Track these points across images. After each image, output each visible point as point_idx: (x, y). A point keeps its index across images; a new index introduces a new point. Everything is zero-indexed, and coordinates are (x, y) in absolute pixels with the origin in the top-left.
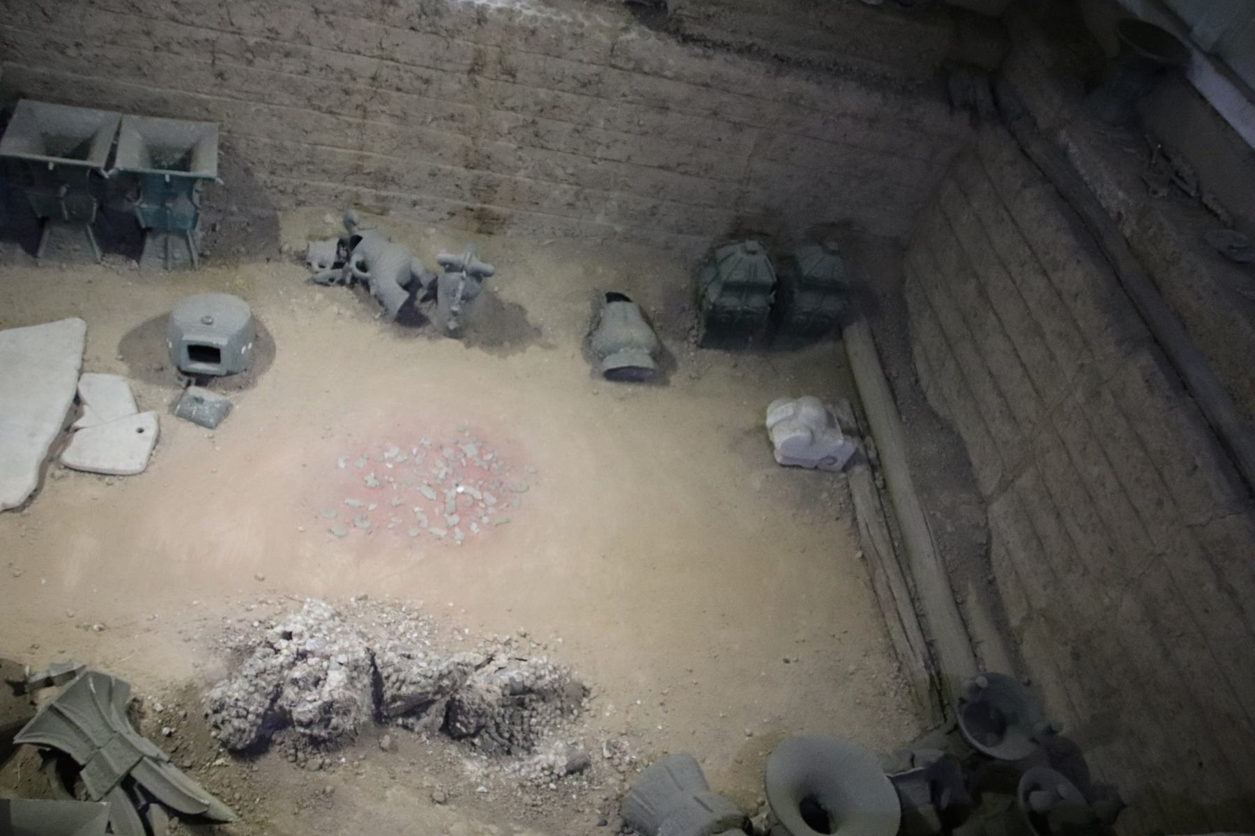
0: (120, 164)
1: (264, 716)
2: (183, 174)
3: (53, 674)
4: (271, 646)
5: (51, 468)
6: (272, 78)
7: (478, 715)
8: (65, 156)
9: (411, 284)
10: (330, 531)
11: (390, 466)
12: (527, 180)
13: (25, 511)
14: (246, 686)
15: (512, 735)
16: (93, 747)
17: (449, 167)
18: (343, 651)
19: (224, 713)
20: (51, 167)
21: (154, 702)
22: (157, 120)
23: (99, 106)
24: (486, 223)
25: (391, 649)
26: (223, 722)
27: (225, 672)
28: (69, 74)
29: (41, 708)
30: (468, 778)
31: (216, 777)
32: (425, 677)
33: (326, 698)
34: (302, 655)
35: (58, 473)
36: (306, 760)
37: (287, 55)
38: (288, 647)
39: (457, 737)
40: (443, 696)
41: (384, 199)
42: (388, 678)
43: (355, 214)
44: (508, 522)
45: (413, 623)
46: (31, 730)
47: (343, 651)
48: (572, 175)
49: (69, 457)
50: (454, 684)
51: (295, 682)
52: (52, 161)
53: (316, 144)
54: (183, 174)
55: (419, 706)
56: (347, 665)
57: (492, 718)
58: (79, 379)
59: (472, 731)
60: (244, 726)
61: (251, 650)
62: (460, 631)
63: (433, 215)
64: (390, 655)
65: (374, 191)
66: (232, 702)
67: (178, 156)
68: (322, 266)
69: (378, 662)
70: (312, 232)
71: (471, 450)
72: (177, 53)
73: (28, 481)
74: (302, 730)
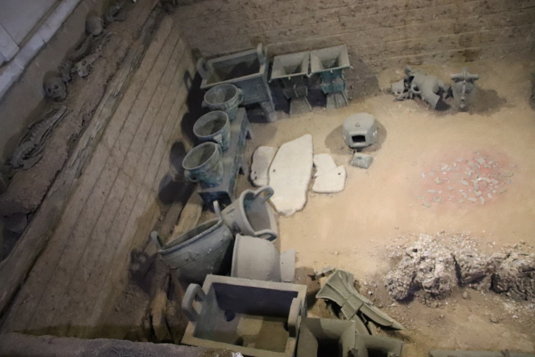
0: (313, 71)
1: (410, 285)
2: (337, 68)
3: (324, 272)
4: (409, 255)
5: (310, 193)
6: (364, 20)
7: (508, 282)
8: (293, 73)
9: (439, 92)
10: (423, 205)
11: (445, 173)
12: (487, 31)
13: (304, 211)
14: (401, 273)
15: (526, 291)
16: (344, 299)
17: (447, 36)
18: (440, 255)
19: (393, 285)
20: (289, 78)
21: (363, 281)
22: (323, 50)
23: (301, 51)
24: (468, 56)
25: (462, 253)
26: (393, 288)
27: (389, 268)
28: (289, 42)
29: (322, 285)
30: (507, 311)
31: (393, 311)
32: (480, 265)
33: (436, 276)
34: (423, 259)
35: (312, 195)
36: (430, 304)
37: (368, 8)
38: (416, 255)
39: (498, 292)
40: (490, 273)
41: (420, 57)
42: (462, 266)
43: (409, 67)
44: (506, 191)
45: (468, 242)
46: (321, 293)
47: (440, 255)
48: (510, 21)
49: (315, 188)
50: (495, 267)
51: (421, 270)
52: (289, 76)
53: (386, 42)
54: (337, 68)
55: (478, 278)
56: (443, 261)
57: (515, 283)
58: (313, 157)
59: (506, 289)
60: (402, 290)
61: (399, 258)
62: (491, 244)
63: (444, 59)
64: (462, 256)
65: (415, 55)
66: (396, 280)
67: (333, 62)
68: (399, 93)
69: (457, 259)
70: (392, 79)
71: (482, 161)
72: (326, 21)
73: (303, 200)
74: (427, 290)
